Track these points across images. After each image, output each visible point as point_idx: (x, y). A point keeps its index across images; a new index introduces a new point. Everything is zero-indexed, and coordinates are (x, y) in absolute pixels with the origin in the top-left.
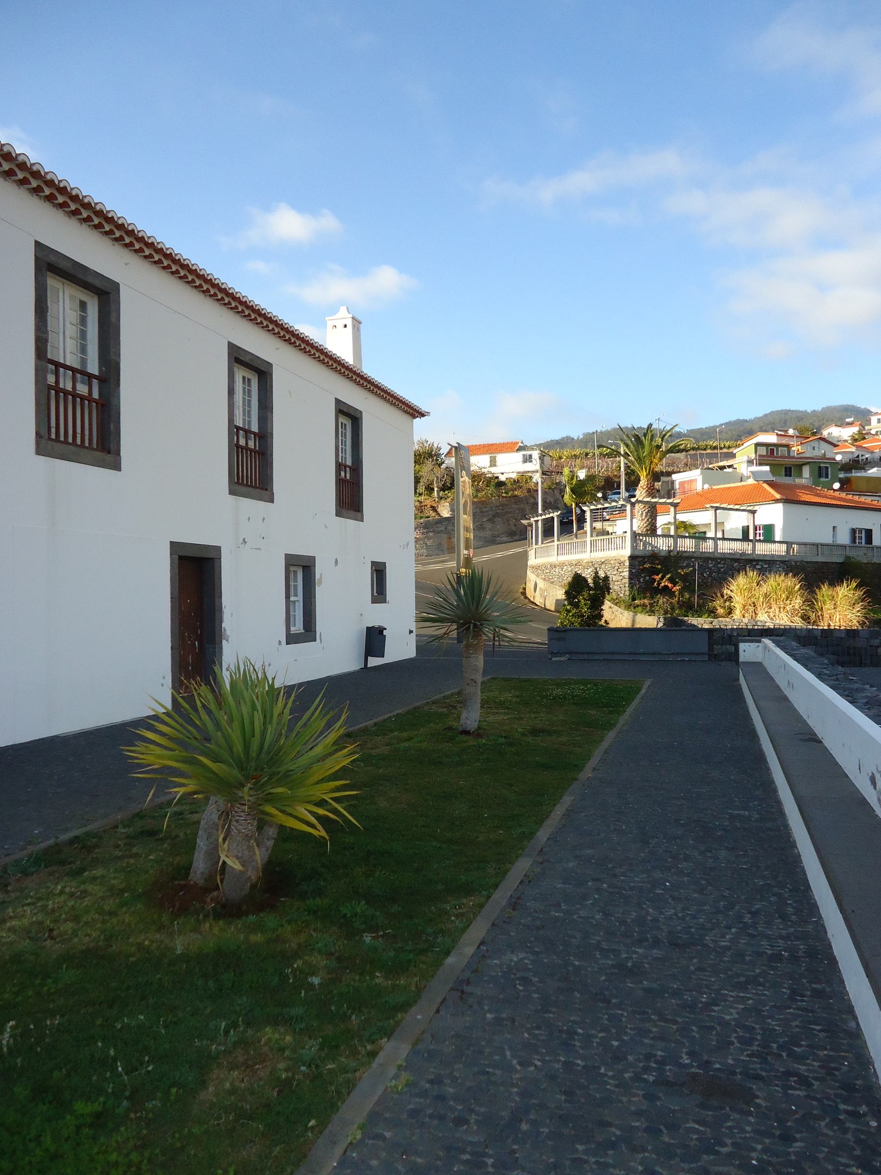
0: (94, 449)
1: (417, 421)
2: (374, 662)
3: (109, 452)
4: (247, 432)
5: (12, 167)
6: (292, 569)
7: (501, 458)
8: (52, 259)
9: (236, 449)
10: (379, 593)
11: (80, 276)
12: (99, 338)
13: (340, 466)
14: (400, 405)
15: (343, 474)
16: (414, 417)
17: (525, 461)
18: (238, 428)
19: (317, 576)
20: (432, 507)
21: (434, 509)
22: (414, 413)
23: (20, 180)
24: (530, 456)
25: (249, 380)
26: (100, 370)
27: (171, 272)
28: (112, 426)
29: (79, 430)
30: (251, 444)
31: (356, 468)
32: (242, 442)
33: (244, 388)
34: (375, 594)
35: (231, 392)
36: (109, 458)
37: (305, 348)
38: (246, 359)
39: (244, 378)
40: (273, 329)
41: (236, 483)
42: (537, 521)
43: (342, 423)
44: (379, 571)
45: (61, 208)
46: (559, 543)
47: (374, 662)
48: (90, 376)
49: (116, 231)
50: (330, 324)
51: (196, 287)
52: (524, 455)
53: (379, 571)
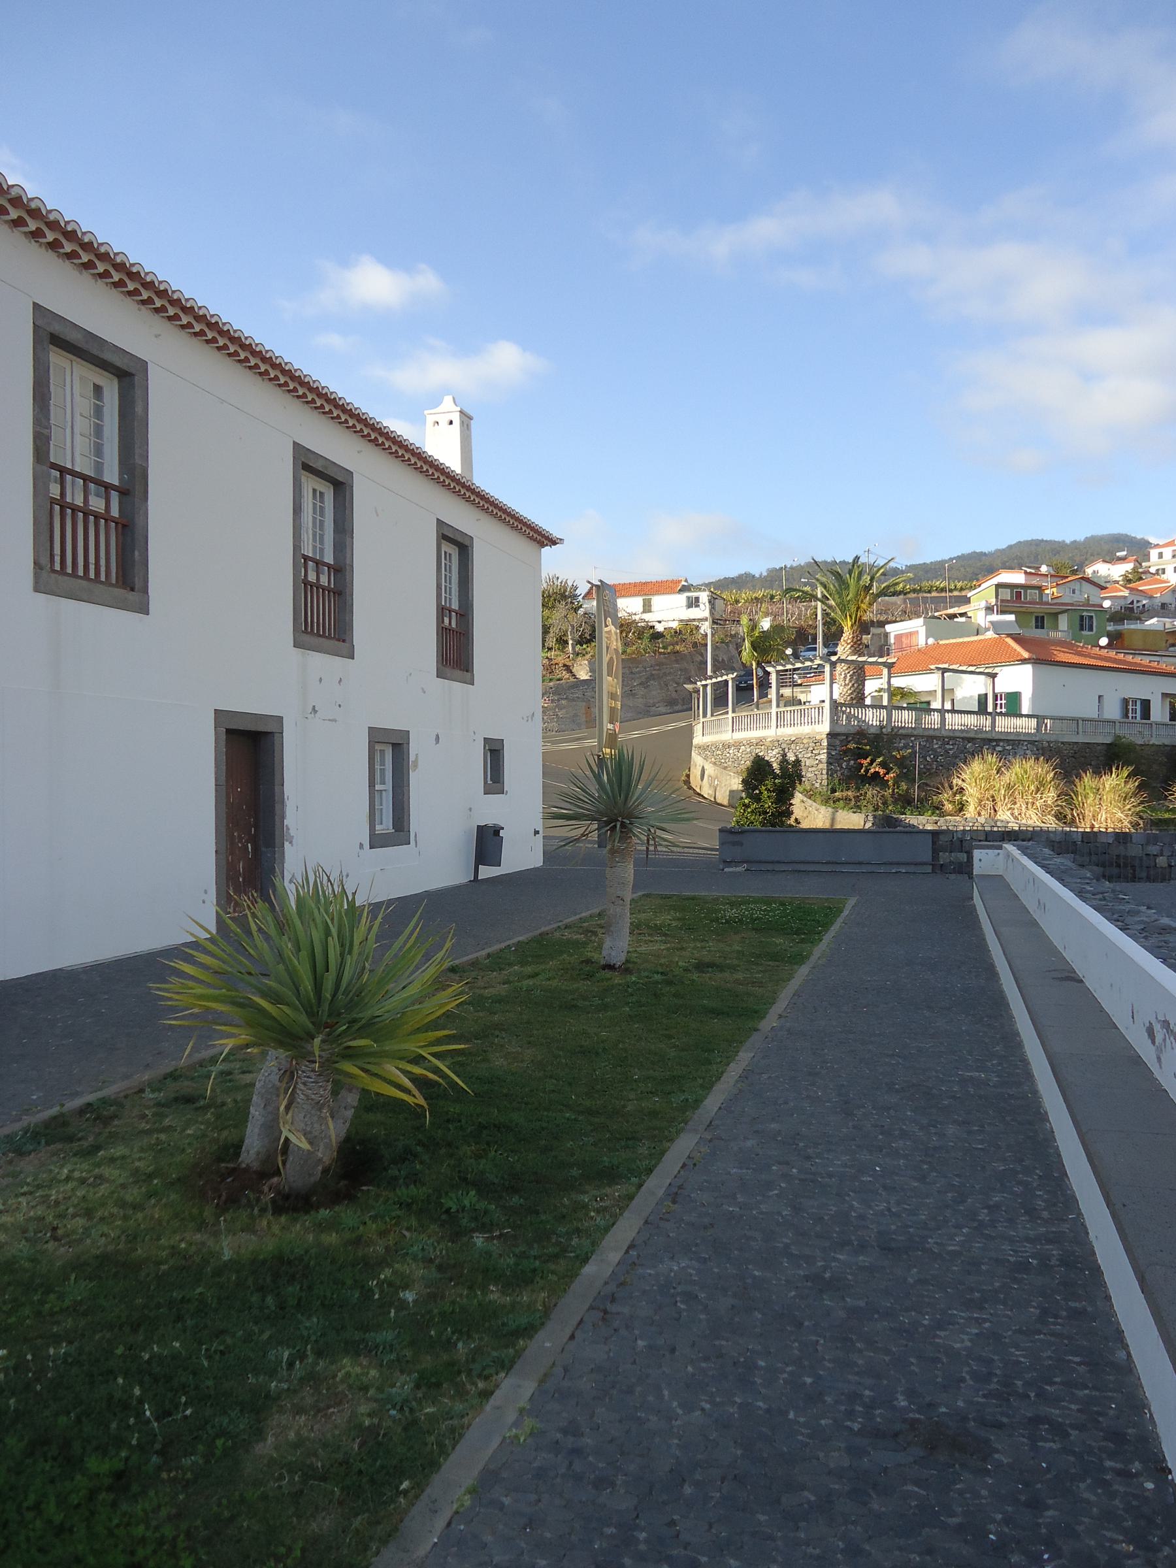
1: (546, 551)
2: (486, 872)
3: (132, 589)
4: (318, 563)
6: (378, 747)
7: (658, 601)
8: (56, 328)
9: (304, 587)
10: (495, 779)
11: (95, 352)
13: (442, 611)
15: (446, 620)
16: (543, 545)
17: (690, 605)
18: (306, 558)
19: (412, 758)
20: (565, 665)
21: (568, 668)
22: (543, 539)
24: (697, 599)
27: (362, 436)
29: (92, 559)
30: (324, 580)
31: (465, 614)
32: (312, 577)
35: (297, 510)
36: (132, 596)
38: (318, 465)
39: (314, 491)
42: (705, 686)
44: (494, 752)
46: (734, 715)
47: (486, 872)
48: (108, 487)
49: (219, 339)
50: (430, 420)
52: (688, 598)
53: (494, 752)
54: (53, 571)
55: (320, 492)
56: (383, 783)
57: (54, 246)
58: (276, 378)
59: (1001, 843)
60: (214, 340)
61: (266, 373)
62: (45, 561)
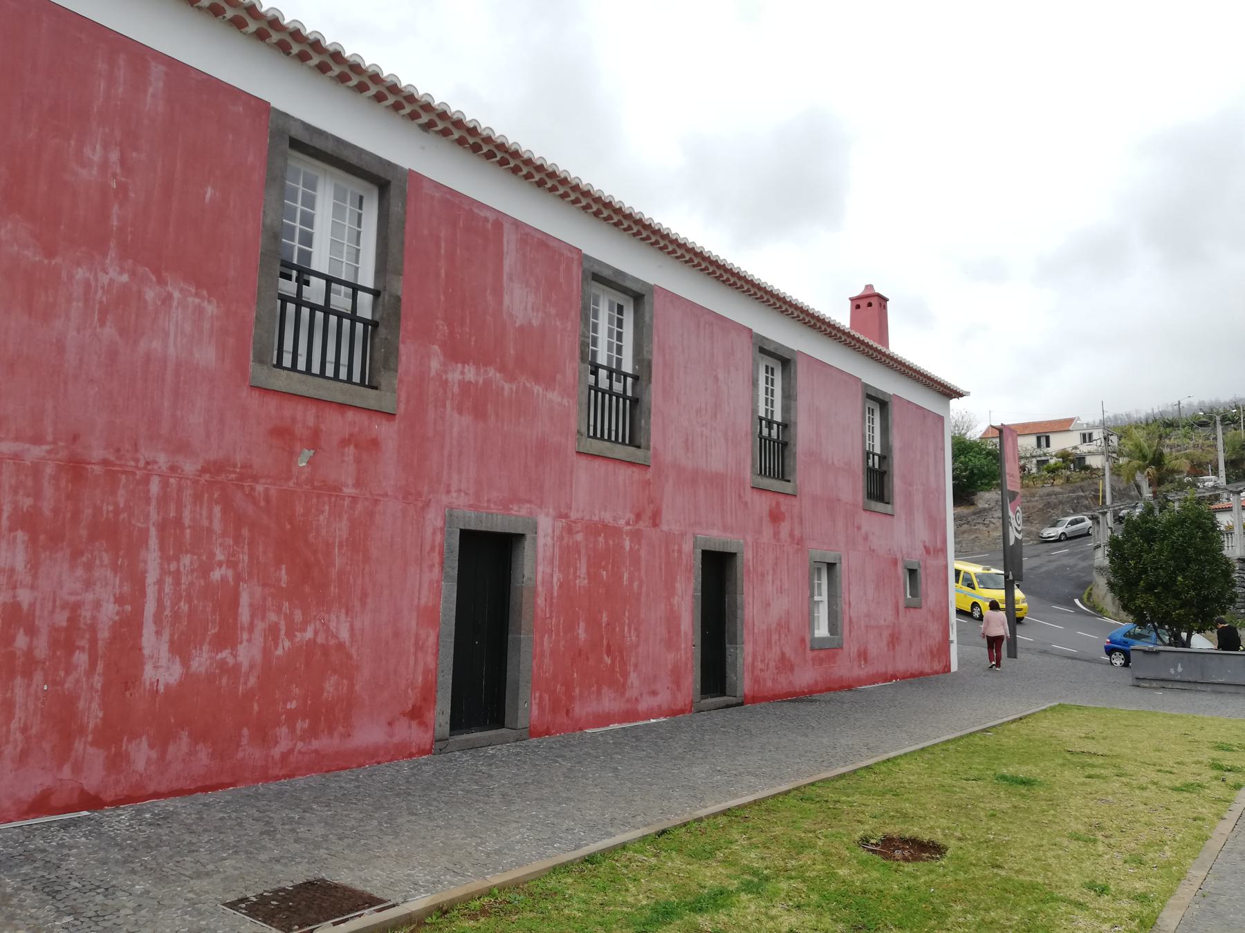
0: (626, 445)
1: (954, 403)
3: (639, 447)
5: (283, 38)
8: (596, 269)
9: (870, 471)
11: (620, 282)
12: (634, 339)
14: (921, 378)
15: (870, 461)
16: (951, 398)
22: (949, 393)
23: (536, 182)
25: (772, 369)
26: (634, 369)
28: (643, 421)
29: (613, 428)
33: (767, 378)
34: (909, 596)
37: (831, 333)
38: (771, 348)
39: (767, 367)
40: (798, 316)
41: (274, 366)
43: (869, 408)
45: (342, 83)
48: (626, 375)
49: (614, 216)
51: (730, 285)
54: (589, 436)
55: (618, 305)
56: (820, 595)
57: (597, 214)
58: (742, 287)
59: (853, 333)
60: (699, 265)
61: (735, 284)
62: (584, 430)
